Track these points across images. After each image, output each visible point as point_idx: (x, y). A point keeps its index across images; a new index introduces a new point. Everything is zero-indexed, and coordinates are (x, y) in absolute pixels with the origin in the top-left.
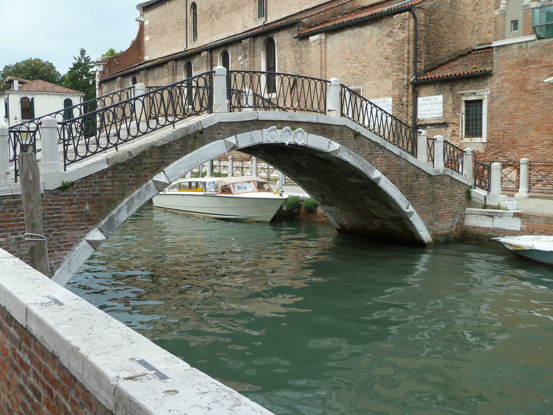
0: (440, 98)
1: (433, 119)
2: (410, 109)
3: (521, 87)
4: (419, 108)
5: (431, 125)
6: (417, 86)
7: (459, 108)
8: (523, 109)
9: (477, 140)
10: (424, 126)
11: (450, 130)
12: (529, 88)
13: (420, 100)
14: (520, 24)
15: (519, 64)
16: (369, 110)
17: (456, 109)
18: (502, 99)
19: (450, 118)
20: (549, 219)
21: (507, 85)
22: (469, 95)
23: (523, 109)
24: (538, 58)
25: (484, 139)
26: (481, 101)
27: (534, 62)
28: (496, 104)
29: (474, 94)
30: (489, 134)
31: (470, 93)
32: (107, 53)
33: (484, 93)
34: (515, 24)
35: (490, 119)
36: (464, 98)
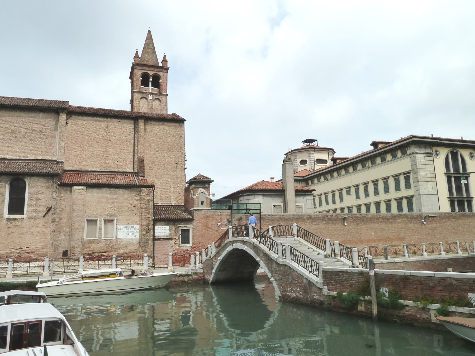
0: (168, 227)
1: (164, 236)
2: (152, 231)
3: (206, 226)
4: (156, 231)
5: (163, 239)
6: (155, 222)
7: (178, 232)
8: (207, 233)
9: (187, 245)
10: (159, 240)
11: (174, 241)
12: (209, 226)
13: (156, 228)
14: (205, 203)
15: (204, 217)
16: (311, 262)
17: (176, 232)
18: (198, 229)
19: (173, 235)
20: (474, 338)
21: (200, 224)
22: (183, 227)
23: (207, 233)
24: (212, 216)
25: (191, 244)
26: (189, 230)
27: (210, 217)
28: (195, 232)
29: (186, 227)
30: (193, 243)
31: (184, 227)
32: (456, 316)
33: (190, 227)
34: (202, 203)
35: (193, 237)
36: (181, 228)
